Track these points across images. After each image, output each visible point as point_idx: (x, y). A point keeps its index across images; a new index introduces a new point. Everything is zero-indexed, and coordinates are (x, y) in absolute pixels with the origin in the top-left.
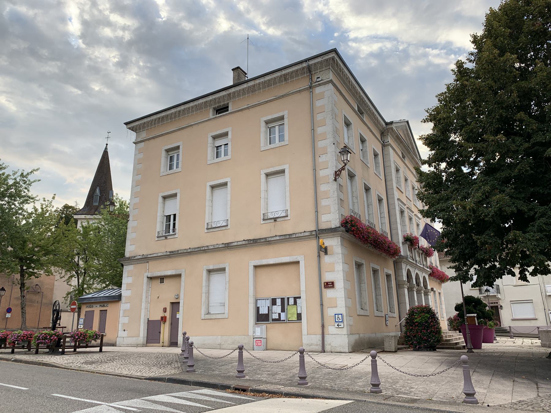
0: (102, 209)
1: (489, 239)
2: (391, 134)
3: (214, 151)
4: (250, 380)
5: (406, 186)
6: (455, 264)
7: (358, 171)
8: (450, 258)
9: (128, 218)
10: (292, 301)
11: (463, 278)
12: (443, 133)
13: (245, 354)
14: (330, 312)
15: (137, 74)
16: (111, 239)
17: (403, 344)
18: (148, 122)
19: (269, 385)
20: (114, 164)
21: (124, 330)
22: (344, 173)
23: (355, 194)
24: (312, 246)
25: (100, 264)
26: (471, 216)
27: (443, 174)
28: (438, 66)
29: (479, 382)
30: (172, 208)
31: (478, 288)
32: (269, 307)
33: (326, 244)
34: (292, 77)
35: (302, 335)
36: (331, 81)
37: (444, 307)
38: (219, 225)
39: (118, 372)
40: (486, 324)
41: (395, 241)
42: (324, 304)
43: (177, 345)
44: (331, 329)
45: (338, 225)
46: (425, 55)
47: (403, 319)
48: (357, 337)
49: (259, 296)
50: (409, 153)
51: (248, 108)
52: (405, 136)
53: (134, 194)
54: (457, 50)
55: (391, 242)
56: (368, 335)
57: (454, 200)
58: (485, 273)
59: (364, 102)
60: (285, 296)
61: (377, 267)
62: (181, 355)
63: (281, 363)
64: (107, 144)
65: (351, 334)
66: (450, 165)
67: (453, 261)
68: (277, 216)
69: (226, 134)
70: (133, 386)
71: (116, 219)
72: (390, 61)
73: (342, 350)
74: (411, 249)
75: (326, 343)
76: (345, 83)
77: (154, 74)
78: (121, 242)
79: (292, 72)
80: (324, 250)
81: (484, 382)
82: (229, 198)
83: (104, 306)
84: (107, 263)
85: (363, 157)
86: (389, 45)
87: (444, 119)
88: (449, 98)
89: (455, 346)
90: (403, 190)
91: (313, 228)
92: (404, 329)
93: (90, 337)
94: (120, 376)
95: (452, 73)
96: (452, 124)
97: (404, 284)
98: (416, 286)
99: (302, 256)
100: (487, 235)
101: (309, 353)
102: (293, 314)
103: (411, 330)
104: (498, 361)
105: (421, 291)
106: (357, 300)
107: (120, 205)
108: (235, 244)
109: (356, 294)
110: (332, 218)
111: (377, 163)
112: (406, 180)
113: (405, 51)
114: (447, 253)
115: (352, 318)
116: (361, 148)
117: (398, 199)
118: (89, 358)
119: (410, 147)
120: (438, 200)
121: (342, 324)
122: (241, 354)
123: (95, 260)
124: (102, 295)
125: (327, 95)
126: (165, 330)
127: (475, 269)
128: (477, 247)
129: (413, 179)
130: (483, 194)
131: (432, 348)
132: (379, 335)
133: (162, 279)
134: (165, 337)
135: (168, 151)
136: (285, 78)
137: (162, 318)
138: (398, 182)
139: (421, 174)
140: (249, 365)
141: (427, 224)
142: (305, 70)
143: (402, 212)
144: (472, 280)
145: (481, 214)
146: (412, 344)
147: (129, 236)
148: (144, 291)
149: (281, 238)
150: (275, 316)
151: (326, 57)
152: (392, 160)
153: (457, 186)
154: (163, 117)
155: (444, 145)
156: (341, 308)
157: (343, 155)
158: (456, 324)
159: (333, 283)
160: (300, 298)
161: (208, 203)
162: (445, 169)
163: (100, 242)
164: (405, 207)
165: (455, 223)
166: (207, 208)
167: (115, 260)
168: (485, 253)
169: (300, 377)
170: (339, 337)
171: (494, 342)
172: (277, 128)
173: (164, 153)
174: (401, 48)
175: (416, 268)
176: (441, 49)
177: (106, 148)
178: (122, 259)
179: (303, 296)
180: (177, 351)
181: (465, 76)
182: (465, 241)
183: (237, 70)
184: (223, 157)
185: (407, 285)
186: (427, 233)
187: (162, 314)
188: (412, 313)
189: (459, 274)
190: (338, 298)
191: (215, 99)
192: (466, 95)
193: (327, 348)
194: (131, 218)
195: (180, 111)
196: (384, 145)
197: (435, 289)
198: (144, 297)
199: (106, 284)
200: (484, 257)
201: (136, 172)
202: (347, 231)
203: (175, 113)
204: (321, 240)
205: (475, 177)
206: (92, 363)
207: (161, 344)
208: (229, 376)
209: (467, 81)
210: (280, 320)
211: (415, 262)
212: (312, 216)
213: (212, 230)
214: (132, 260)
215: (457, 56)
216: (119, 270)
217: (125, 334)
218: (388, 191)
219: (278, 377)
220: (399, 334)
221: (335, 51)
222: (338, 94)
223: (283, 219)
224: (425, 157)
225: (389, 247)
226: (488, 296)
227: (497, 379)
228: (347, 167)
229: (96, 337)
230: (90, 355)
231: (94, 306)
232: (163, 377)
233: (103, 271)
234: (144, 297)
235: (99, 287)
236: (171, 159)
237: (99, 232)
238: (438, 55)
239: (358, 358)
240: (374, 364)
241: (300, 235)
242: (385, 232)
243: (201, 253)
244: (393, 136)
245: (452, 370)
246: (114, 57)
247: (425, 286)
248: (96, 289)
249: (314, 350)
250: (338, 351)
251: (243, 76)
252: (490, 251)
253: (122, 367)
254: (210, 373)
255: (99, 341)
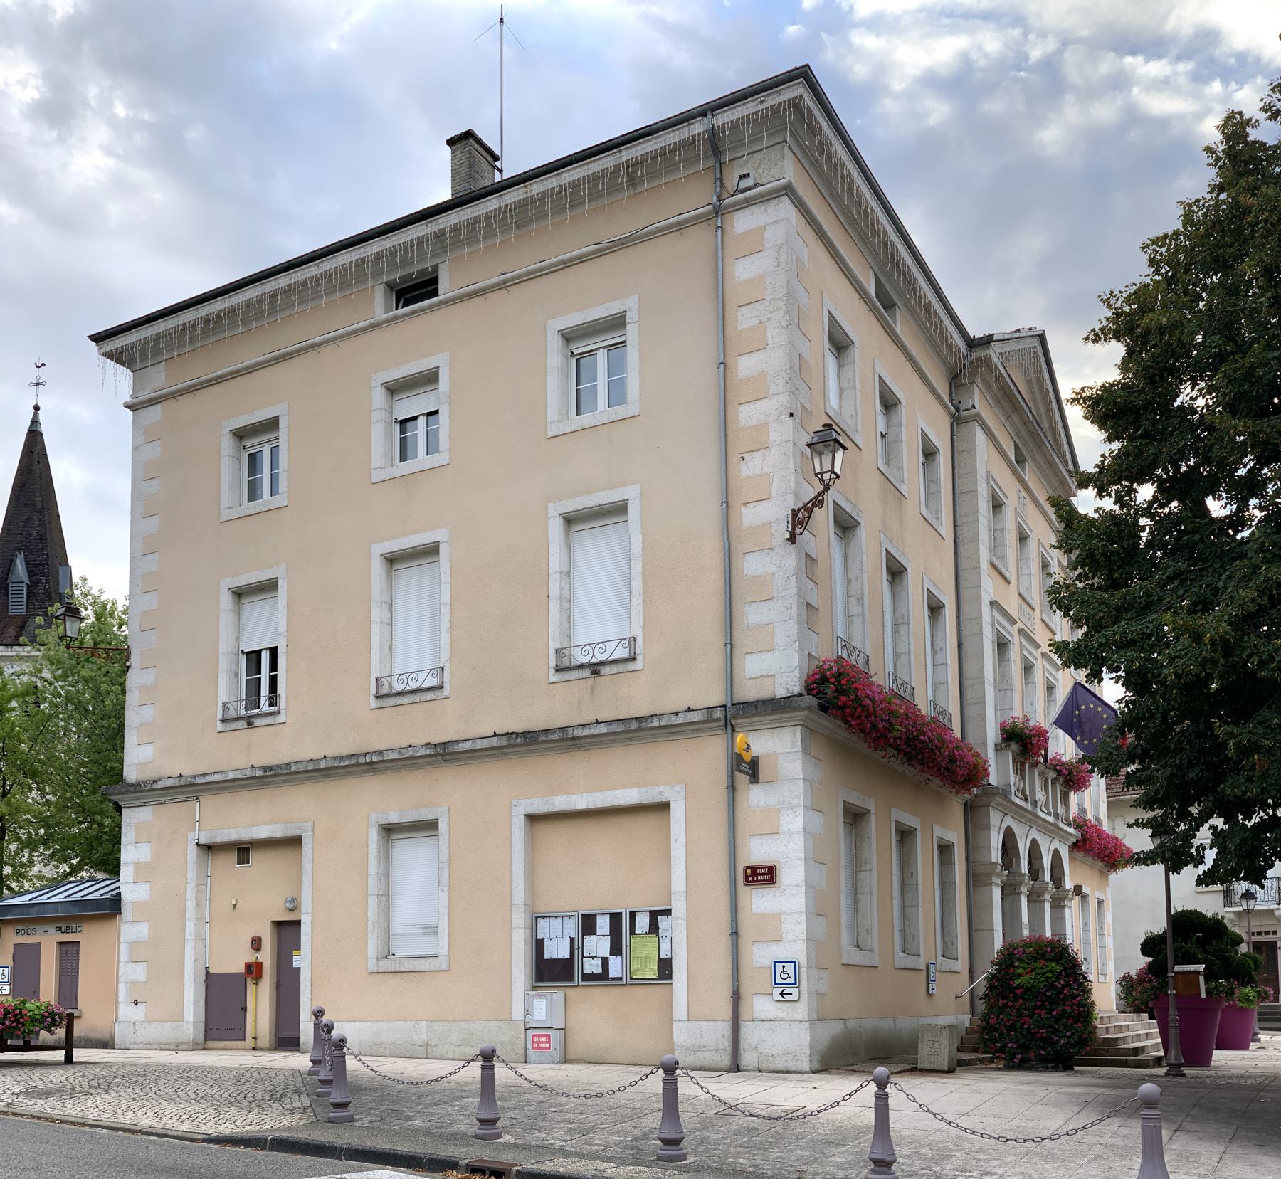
0: (40, 627)
1: (1264, 736)
2: (984, 381)
3: (392, 436)
4: (515, 1145)
5: (1022, 557)
6: (1151, 814)
7: (869, 512)
8: (1136, 793)
9: (128, 658)
10: (643, 923)
11: (1174, 855)
12: (1151, 381)
13: (501, 1072)
14: (760, 956)
15: (109, 151)
16: (78, 725)
17: (975, 1050)
18: (170, 334)
19: (570, 1160)
20: (65, 473)
21: (136, 1003)
22: (823, 518)
23: (854, 587)
24: (710, 754)
25: (48, 803)
26: (1215, 662)
27: (1143, 521)
28: (1162, 123)
29: (1187, 1158)
30: (264, 626)
31: (1219, 887)
32: (572, 940)
33: (756, 750)
34: (654, 175)
35: (671, 1020)
36: (788, 190)
37: (1109, 942)
38: (414, 686)
39: (125, 1119)
40: (1231, 992)
41: (972, 739)
42: (742, 931)
43: (298, 1044)
44: (762, 1005)
45: (796, 689)
46: (1119, 82)
47: (981, 979)
48: (836, 1028)
49: (542, 908)
50: (1040, 446)
51: (503, 285)
52: (1031, 389)
53: (140, 581)
54: (1232, 61)
55: (962, 744)
56: (868, 1019)
57: (1165, 611)
58: (1243, 841)
59: (898, 264)
60: (624, 907)
61: (910, 820)
62: (310, 1073)
63: (607, 1098)
64: (37, 408)
65: (819, 1019)
66: (1166, 492)
67: (1147, 803)
68: (600, 657)
69: (430, 378)
70: (172, 1161)
71: (87, 660)
72: (994, 106)
73: (792, 1065)
74: (1023, 765)
75: (743, 1044)
76: (829, 185)
77: (166, 150)
78: (109, 735)
79: (654, 156)
80: (748, 768)
81: (1202, 1160)
82: (445, 598)
83: (68, 930)
84: (71, 799)
85: (888, 461)
86: (992, 42)
87: (1162, 331)
88: (1189, 252)
89: (1132, 1058)
90: (1011, 573)
91: (714, 696)
92: (981, 1006)
93: (33, 1019)
94: (133, 1132)
95: (1206, 159)
96: (1186, 346)
97: (990, 875)
98: (1027, 878)
99: (679, 788)
100: (1260, 723)
101: (692, 1074)
102: (646, 960)
103: (1002, 1010)
104: (1253, 1100)
105: (1042, 893)
106: (844, 918)
107: (98, 616)
108: (468, 746)
109: (837, 905)
110: (777, 668)
111: (931, 481)
112: (1023, 538)
113: (1050, 67)
114: (1131, 781)
115: (824, 974)
116: (881, 428)
117: (993, 604)
118: (37, 1079)
119: (1046, 425)
120: (1118, 610)
121: (794, 991)
122: (488, 1074)
123: (31, 789)
124: (61, 898)
125: (771, 244)
126: (260, 1006)
127: (1214, 828)
128: (1227, 760)
129: (1044, 533)
130: (1261, 593)
131: (1061, 1061)
132: (905, 1024)
133: (243, 850)
134: (260, 1022)
135: (240, 435)
136: (631, 176)
137: (249, 967)
138: (997, 546)
139: (1068, 516)
140: (512, 1104)
141: (1078, 685)
142: (701, 147)
143: (1002, 646)
144: (1199, 861)
145: (1250, 656)
146: (1002, 1050)
147: (135, 717)
148: (191, 887)
149: (614, 728)
150: (593, 966)
151: (773, 99)
152: (981, 470)
153: (1181, 566)
154: (218, 316)
155: (1155, 422)
156: (794, 946)
157: (820, 454)
158: (1140, 995)
159: (771, 870)
160: (668, 912)
161: (377, 614)
162: (1150, 503)
163: (41, 733)
164: (1014, 630)
165: (1162, 683)
166: (375, 629)
167: (94, 793)
168: (1250, 779)
169: (663, 1140)
170: (783, 1028)
171: (1252, 1046)
172: (602, 356)
173: (227, 443)
174: (1036, 54)
175: (1035, 823)
176: (1179, 58)
177: (35, 422)
178: (116, 788)
179: (678, 907)
180: (300, 1061)
181: (1251, 173)
182: (1189, 743)
183: (463, 141)
184: (421, 459)
185: (999, 875)
186: (1076, 716)
187: (250, 957)
188: (1008, 959)
189: (1161, 846)
190: (785, 916)
191: (392, 252)
192: (1245, 242)
193: (748, 1058)
194: (134, 661)
195: (273, 296)
196: (959, 419)
197: (1085, 890)
198: (190, 905)
199: (71, 866)
200: (1244, 792)
201: (143, 507)
202: (824, 708)
203: (259, 302)
204: (739, 738)
205: (1245, 534)
206: (45, 1094)
207: (249, 1042)
208: (453, 1134)
209: (1253, 190)
210: (607, 978)
211: (1029, 807)
212: (715, 658)
213: (392, 701)
214: (146, 791)
215: (1233, 86)
216: (107, 821)
217: (138, 1013)
218: (963, 575)
219: (597, 1138)
220: (966, 1020)
221: (803, 74)
222: (810, 235)
223: (621, 667)
224: (1088, 463)
225: (953, 760)
226: (1248, 911)
227: (1240, 1151)
228: (831, 496)
229: (50, 1019)
230: (38, 1072)
231: (40, 929)
232: (260, 1135)
233: (58, 824)
234: (190, 905)
235: (49, 872)
236: (254, 460)
237: (37, 703)
238: (1163, 84)
239: (836, 1087)
240: (882, 1103)
241: (674, 720)
242: (943, 712)
243: (362, 772)
244: (989, 388)
245: (1112, 1125)
246: (23, 83)
247: (1058, 879)
248: (40, 878)
249: (707, 1063)
250: (780, 1067)
251: (485, 166)
252: (1264, 777)
253: (135, 1105)
254: (396, 1125)
255: (61, 1033)
